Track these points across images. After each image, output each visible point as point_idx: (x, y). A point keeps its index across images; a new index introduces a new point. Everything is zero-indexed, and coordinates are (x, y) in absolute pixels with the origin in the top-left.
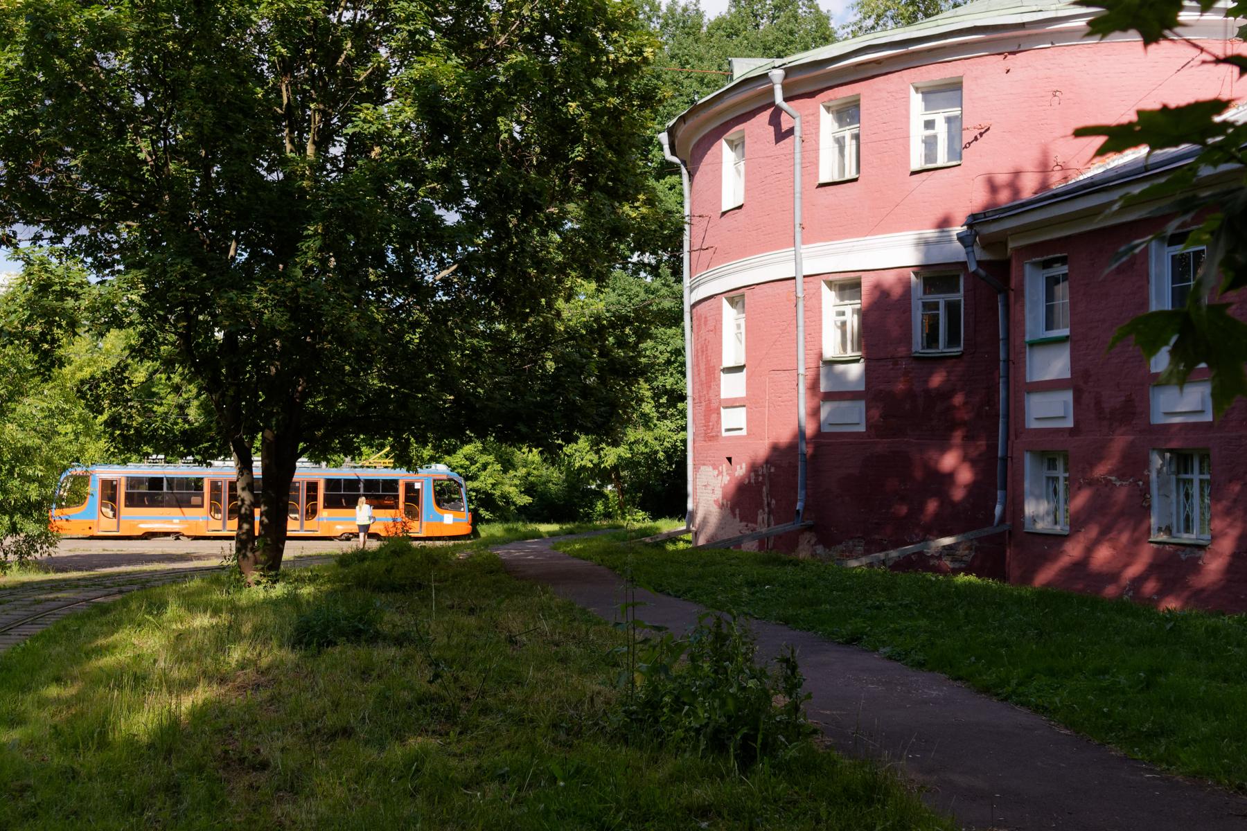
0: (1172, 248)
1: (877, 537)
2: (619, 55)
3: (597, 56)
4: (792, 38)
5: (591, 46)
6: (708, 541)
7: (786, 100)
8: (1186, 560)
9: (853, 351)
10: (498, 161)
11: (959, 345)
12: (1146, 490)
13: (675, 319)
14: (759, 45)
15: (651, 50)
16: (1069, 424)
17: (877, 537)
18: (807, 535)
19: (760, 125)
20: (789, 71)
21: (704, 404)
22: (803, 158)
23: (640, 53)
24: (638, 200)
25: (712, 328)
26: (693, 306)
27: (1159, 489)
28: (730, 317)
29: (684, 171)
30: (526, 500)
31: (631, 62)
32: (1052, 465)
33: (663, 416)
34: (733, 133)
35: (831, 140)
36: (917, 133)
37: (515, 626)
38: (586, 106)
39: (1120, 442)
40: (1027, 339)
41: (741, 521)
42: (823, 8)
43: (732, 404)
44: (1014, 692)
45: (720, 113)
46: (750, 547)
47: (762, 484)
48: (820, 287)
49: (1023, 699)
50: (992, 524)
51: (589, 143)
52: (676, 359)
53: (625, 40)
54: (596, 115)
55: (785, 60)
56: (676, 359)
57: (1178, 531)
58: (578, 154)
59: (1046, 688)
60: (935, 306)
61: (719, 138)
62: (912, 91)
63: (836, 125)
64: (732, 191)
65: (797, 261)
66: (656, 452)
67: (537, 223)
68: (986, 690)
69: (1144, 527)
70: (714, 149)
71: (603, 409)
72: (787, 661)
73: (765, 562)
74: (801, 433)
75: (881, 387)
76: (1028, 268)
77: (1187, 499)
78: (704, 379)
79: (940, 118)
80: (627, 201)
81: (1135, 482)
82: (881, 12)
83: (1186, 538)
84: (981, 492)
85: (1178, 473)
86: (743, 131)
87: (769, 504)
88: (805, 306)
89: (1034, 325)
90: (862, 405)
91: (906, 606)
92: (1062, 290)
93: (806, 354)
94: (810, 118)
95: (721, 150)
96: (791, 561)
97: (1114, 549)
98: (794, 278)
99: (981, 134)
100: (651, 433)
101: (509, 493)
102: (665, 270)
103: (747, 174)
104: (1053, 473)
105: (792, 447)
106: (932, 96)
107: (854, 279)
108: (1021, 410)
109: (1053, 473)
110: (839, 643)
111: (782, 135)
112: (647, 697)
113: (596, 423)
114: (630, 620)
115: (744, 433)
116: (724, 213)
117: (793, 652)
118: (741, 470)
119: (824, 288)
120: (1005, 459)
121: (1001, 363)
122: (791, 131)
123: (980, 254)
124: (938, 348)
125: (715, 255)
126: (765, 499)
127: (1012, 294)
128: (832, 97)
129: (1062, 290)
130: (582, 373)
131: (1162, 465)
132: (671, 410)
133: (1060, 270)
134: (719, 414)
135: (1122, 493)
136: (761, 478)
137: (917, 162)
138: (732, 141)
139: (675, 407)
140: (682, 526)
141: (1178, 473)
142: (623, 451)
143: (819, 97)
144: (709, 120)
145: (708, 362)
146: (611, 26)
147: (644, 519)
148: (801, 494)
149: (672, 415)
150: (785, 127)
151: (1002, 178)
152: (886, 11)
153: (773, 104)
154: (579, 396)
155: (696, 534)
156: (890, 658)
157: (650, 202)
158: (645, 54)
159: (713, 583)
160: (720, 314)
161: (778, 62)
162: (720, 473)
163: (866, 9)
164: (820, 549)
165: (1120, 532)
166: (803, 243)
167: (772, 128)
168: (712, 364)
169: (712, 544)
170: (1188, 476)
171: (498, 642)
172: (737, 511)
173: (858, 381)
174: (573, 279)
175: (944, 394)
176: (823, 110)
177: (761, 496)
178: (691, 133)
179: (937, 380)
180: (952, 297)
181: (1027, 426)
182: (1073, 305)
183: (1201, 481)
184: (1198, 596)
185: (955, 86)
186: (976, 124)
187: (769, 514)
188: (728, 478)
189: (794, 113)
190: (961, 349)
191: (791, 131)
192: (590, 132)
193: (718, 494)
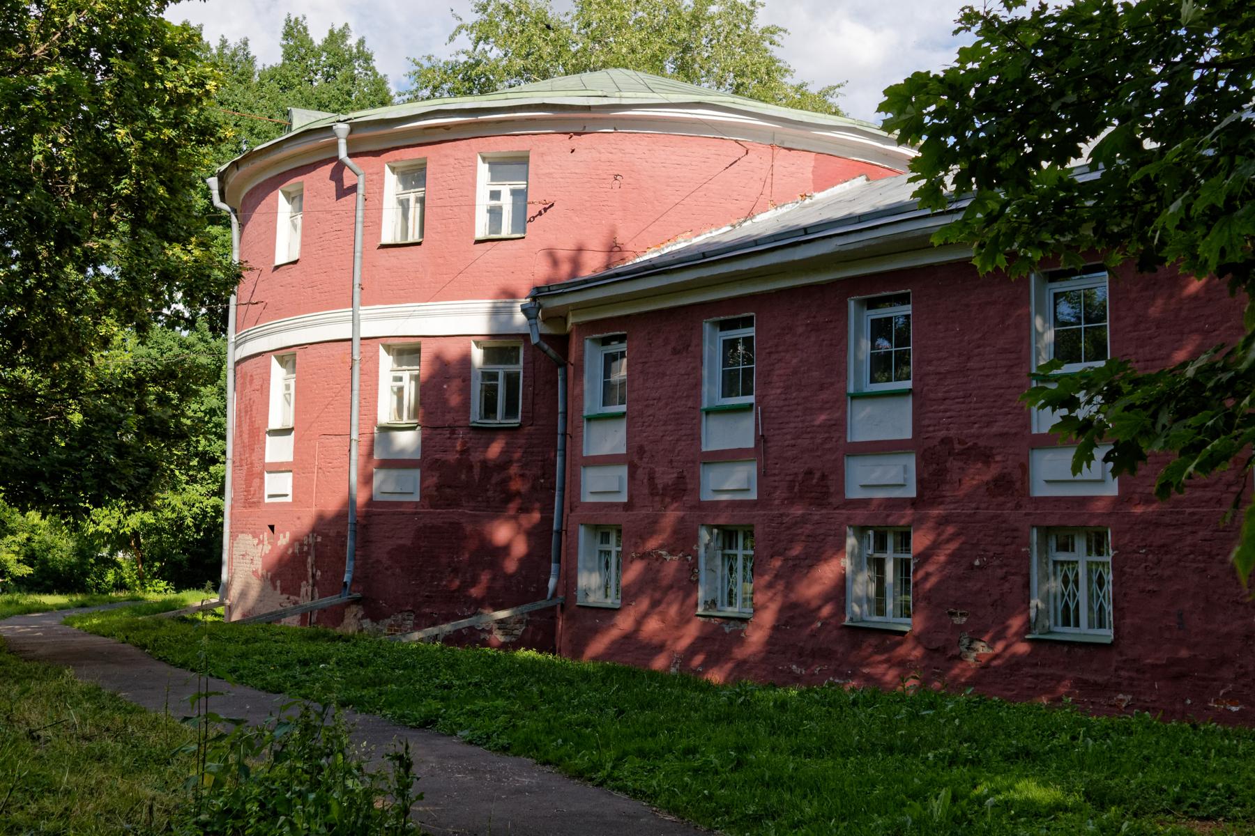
1: (428, 610)
2: (178, 84)
3: (151, 82)
4: (348, 98)
5: (146, 71)
6: (244, 615)
7: (350, 155)
8: (730, 633)
9: (409, 418)
10: (32, 184)
11: (516, 416)
12: (695, 565)
13: (214, 375)
14: (314, 102)
15: (214, 83)
17: (428, 610)
18: (354, 609)
19: (321, 178)
20: (355, 127)
21: (245, 467)
22: (365, 216)
23: (202, 85)
24: (191, 243)
26: (237, 363)
27: (706, 564)
28: (279, 376)
29: (234, 219)
30: (26, 570)
31: (190, 95)
32: (605, 538)
33: (193, 480)
35: (395, 201)
36: (483, 202)
37: (34, 717)
38: (137, 135)
39: (671, 516)
40: (585, 413)
41: (282, 594)
42: (381, 71)
43: (277, 468)
44: (609, 776)
45: (277, 163)
46: (293, 621)
47: (308, 553)
48: (378, 351)
49: (619, 783)
50: (545, 597)
51: (139, 175)
52: (210, 418)
53: (186, 69)
54: (147, 146)
55: (351, 115)
56: (210, 418)
57: (723, 605)
58: (125, 186)
59: (640, 770)
60: (494, 376)
61: (275, 188)
62: (479, 159)
63: (401, 187)
64: (287, 245)
65: (355, 322)
66: (183, 519)
67: (72, 257)
68: (579, 775)
69: (691, 601)
70: (269, 199)
71: (141, 470)
72: (400, 758)
73: (313, 638)
74: (350, 501)
75: (437, 456)
77: (731, 574)
78: (246, 441)
79: (505, 190)
80: (178, 242)
81: (684, 556)
82: (437, 83)
83: (730, 611)
84: (536, 563)
85: (724, 548)
87: (314, 576)
88: (361, 369)
89: (592, 402)
90: (416, 474)
91: (476, 684)
93: (360, 419)
94: (375, 177)
95: (277, 201)
96: (340, 636)
97: (663, 622)
98: (351, 340)
99: (545, 210)
100: (179, 498)
101: (6, 561)
102: (203, 325)
103: (304, 228)
104: (605, 547)
105: (341, 516)
106: (500, 168)
107: (415, 344)
108: (577, 485)
109: (605, 547)
110: (412, 727)
111: (344, 192)
112: (225, 804)
113: (131, 486)
114: (203, 712)
115: (289, 499)
116: (277, 267)
117: (407, 747)
118: (284, 540)
119: (382, 352)
120: (559, 533)
122: (354, 189)
124: (496, 418)
125: (267, 311)
126: (310, 570)
127: (571, 369)
130: (118, 429)
131: (710, 541)
132: (203, 474)
133: (615, 347)
134: (262, 479)
135: (672, 564)
136: (306, 548)
137: (481, 231)
138: (289, 193)
139: (207, 470)
140: (214, 598)
141: (724, 548)
142: (149, 518)
143: (384, 156)
144: (264, 169)
145: (252, 423)
146: (170, 51)
147: (166, 590)
148: (349, 566)
149: (203, 478)
150: (347, 183)
151: (564, 253)
152: (442, 83)
153: (336, 158)
154: (113, 454)
155: (230, 609)
156: (470, 742)
157: (204, 245)
158: (208, 87)
159: (260, 662)
160: (268, 373)
161: (342, 117)
163: (423, 79)
164: (367, 623)
165: (669, 604)
166: (362, 304)
167: (333, 184)
169: (247, 619)
170: (733, 552)
171: (15, 740)
172: (278, 583)
173: (413, 453)
174: (109, 325)
175: (502, 465)
176: (387, 170)
177: (305, 566)
178: (244, 180)
179: (495, 450)
180: (512, 368)
183: (746, 558)
184: (742, 666)
185: (521, 160)
186: (541, 199)
187: (313, 586)
188: (270, 547)
189: (358, 171)
190: (519, 420)
191: (354, 189)
192: (139, 163)
193: (259, 565)
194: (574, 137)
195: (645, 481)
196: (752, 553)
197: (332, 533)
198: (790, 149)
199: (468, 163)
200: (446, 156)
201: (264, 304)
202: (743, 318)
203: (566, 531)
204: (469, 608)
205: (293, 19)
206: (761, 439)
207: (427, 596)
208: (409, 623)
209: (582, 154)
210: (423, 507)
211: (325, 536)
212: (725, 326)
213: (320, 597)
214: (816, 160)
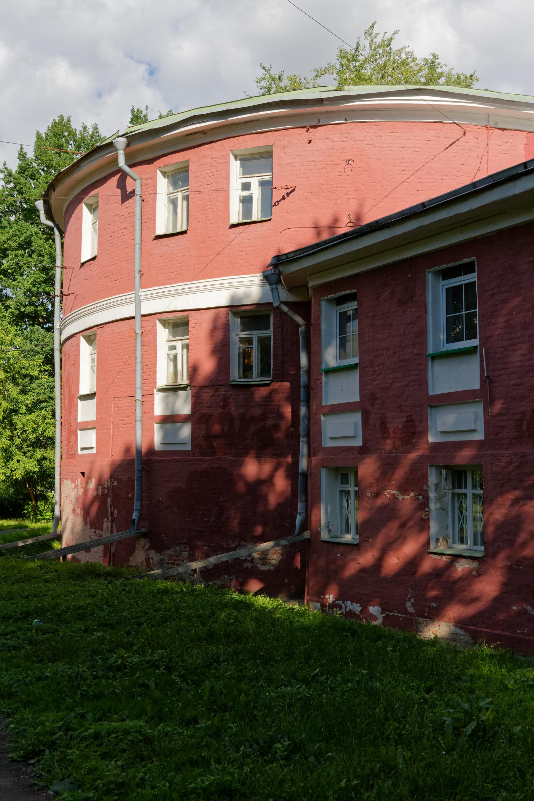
0: (447, 282)
16: (358, 442)
18: (142, 541)
25: (73, 362)
32: (345, 480)
34: (89, 198)
41: (91, 528)
43: (86, 427)
48: (155, 325)
57: (454, 542)
62: (232, 157)
63: (171, 188)
76: (324, 304)
79: (254, 182)
85: (454, 488)
86: (97, 195)
87: (112, 514)
88: (142, 341)
92: (353, 327)
94: (149, 181)
98: (133, 318)
99: (288, 194)
104: (345, 487)
106: (249, 163)
109: (345, 487)
115: (94, 451)
116: (83, 264)
119: (159, 326)
121: (302, 389)
123: (284, 295)
124: (252, 377)
126: (109, 509)
128: (167, 163)
129: (353, 327)
133: (351, 307)
134: (76, 435)
137: (235, 217)
138: (91, 205)
141: (454, 488)
145: (70, 390)
148: (137, 505)
150: (129, 189)
160: (78, 350)
162: (76, 486)
164: (152, 554)
166: (142, 287)
167: (119, 191)
168: (72, 393)
176: (159, 174)
177: (106, 506)
181: (323, 445)
182: (361, 334)
187: (112, 522)
190: (271, 378)
191: (133, 193)
194: (311, 130)
195: (378, 426)
196: (481, 492)
197: (125, 479)
198: (503, 129)
199: (222, 161)
200: (204, 157)
201: (74, 295)
202: (464, 264)
203: (311, 473)
204: (233, 541)
205: (136, 110)
206: (486, 380)
207: (199, 531)
208: (185, 554)
209: (317, 144)
210: (194, 455)
211: (120, 481)
212: (447, 274)
213: (117, 532)
214: (527, 138)
